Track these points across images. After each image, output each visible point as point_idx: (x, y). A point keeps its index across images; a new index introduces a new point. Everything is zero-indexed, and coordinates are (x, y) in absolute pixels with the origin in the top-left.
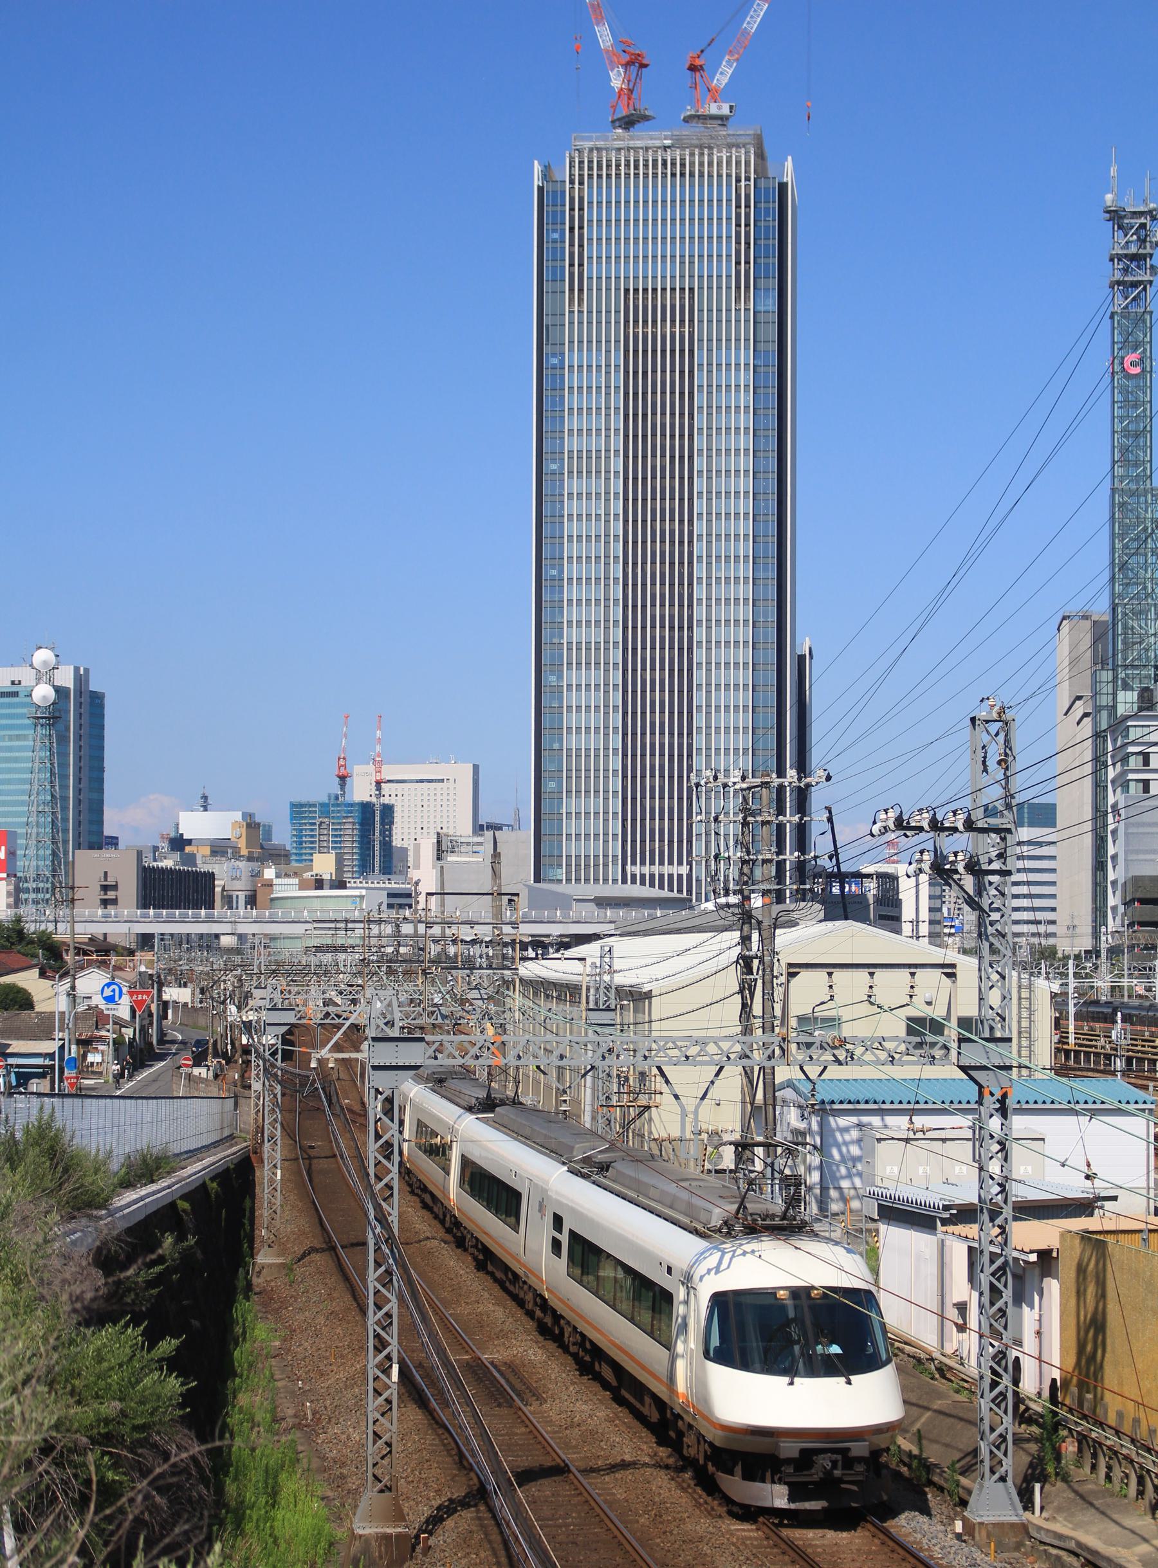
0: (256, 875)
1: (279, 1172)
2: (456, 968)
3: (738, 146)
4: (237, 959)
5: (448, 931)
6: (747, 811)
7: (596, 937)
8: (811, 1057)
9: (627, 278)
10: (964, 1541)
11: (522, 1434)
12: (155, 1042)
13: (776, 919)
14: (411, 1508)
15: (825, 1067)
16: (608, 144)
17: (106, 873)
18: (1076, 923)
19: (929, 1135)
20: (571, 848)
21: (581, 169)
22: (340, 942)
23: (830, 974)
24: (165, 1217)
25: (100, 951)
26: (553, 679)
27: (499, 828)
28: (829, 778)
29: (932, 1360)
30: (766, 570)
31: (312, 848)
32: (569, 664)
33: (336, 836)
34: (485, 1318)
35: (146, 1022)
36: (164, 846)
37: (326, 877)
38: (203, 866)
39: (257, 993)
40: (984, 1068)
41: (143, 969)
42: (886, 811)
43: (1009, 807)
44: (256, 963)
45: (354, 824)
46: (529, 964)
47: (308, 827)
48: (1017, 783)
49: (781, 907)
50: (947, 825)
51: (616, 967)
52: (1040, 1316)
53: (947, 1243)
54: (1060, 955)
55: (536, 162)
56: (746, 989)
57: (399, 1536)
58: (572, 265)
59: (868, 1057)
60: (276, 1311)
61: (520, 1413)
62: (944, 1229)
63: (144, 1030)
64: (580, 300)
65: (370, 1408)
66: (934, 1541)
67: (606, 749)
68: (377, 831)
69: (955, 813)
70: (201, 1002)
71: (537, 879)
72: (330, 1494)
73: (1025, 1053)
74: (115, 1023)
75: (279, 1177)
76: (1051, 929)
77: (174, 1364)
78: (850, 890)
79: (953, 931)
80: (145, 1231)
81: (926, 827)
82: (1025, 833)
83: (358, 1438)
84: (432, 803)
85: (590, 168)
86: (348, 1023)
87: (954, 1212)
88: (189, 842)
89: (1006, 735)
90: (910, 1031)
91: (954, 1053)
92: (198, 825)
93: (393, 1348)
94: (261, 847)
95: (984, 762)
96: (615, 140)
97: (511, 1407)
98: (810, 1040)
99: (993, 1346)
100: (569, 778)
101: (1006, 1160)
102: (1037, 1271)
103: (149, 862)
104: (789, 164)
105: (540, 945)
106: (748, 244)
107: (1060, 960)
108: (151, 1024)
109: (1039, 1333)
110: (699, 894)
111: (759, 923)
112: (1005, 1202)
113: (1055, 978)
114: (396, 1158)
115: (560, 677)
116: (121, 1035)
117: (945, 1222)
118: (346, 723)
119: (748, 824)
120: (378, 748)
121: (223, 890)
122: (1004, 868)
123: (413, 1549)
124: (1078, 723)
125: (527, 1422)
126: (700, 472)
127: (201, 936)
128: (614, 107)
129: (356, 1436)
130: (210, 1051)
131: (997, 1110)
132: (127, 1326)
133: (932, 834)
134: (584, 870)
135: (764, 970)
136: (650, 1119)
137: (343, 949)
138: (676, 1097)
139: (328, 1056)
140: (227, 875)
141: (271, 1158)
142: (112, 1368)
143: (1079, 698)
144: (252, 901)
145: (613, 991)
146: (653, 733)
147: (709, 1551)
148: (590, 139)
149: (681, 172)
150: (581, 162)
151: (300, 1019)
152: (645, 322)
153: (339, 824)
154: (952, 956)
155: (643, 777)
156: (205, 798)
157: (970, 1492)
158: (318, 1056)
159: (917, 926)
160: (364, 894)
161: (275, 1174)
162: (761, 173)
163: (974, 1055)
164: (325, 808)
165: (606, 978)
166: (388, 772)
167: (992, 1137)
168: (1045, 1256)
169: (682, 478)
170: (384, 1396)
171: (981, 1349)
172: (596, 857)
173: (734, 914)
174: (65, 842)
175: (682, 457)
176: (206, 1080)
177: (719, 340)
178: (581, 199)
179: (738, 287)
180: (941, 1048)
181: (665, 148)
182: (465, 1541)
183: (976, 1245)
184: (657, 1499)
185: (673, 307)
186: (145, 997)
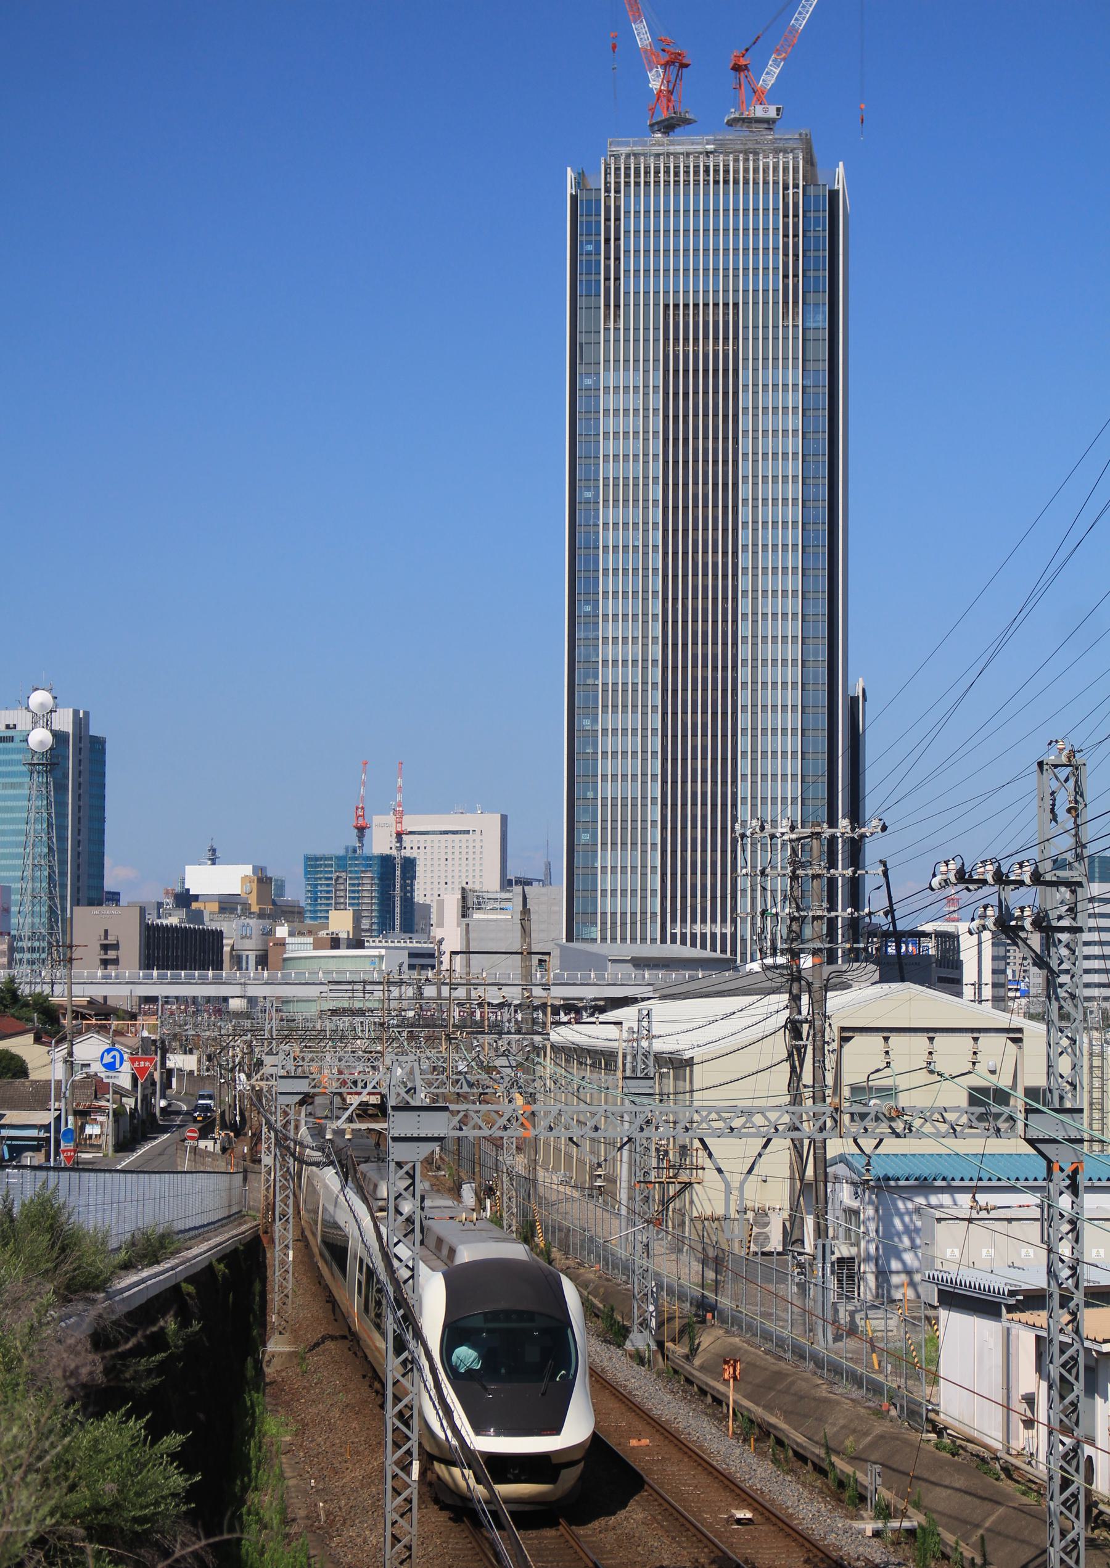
0: (269, 933)
1: (291, 1253)
3: (785, 151)
4: (247, 1024)
5: (474, 994)
6: (796, 864)
8: (866, 1130)
9: (666, 292)
13: (828, 980)
15: (881, 1140)
16: (647, 149)
17: (106, 931)
19: (994, 1214)
20: (605, 905)
21: (617, 176)
22: (358, 1005)
24: (169, 1298)
25: (100, 1014)
26: (587, 723)
27: (528, 883)
28: (884, 828)
29: (997, 1459)
30: (815, 606)
31: (328, 905)
32: (605, 706)
33: (353, 891)
38: (210, 925)
39: (268, 1060)
40: (1054, 1141)
41: (145, 1034)
42: (947, 863)
43: (1079, 857)
44: (267, 1027)
45: (372, 878)
46: (562, 1029)
48: (1088, 832)
49: (832, 968)
50: (1012, 878)
51: (655, 1032)
53: (1013, 1332)
55: (569, 169)
56: (795, 1055)
58: (607, 279)
59: (928, 1128)
60: (288, 1404)
62: (1010, 1316)
63: (146, 1100)
65: (388, 1509)
67: (644, 798)
68: (398, 886)
70: (208, 1070)
71: (570, 938)
74: (115, 1092)
75: (291, 1259)
77: (183, 1459)
81: (990, 880)
83: (374, 1542)
85: (627, 175)
87: (1021, 1298)
88: (196, 898)
89: (1076, 782)
91: (1020, 1125)
92: (212, 880)
94: (270, 901)
96: (654, 145)
98: (864, 1110)
99: (1063, 1444)
100: (604, 829)
101: (1077, 1241)
103: (152, 919)
104: (840, 170)
105: (574, 1009)
106: (796, 255)
110: (744, 954)
112: (1077, 1287)
116: (122, 1105)
117: (1010, 1309)
121: (232, 949)
127: (208, 999)
128: (653, 110)
131: (1067, 1187)
133: (996, 888)
134: (622, 927)
135: (814, 1036)
137: (361, 1012)
138: (720, 1171)
139: (345, 1126)
140: (234, 933)
141: (283, 1238)
142: (110, 1459)
144: (263, 961)
145: (652, 1058)
148: (627, 144)
149: (724, 179)
150: (617, 169)
151: (314, 1087)
153: (358, 878)
154: (1018, 1021)
155: (684, 782)
158: (334, 1127)
159: (980, 989)
160: (383, 954)
161: (287, 1255)
163: (1045, 1126)
164: (342, 862)
165: (644, 1044)
166: (410, 823)
167: (1062, 1216)
171: (1051, 1447)
174: (63, 898)
176: (213, 1153)
177: (765, 359)
180: (1006, 1120)
181: (708, 154)
183: (1044, 1334)
185: (716, 323)
186: (147, 1064)
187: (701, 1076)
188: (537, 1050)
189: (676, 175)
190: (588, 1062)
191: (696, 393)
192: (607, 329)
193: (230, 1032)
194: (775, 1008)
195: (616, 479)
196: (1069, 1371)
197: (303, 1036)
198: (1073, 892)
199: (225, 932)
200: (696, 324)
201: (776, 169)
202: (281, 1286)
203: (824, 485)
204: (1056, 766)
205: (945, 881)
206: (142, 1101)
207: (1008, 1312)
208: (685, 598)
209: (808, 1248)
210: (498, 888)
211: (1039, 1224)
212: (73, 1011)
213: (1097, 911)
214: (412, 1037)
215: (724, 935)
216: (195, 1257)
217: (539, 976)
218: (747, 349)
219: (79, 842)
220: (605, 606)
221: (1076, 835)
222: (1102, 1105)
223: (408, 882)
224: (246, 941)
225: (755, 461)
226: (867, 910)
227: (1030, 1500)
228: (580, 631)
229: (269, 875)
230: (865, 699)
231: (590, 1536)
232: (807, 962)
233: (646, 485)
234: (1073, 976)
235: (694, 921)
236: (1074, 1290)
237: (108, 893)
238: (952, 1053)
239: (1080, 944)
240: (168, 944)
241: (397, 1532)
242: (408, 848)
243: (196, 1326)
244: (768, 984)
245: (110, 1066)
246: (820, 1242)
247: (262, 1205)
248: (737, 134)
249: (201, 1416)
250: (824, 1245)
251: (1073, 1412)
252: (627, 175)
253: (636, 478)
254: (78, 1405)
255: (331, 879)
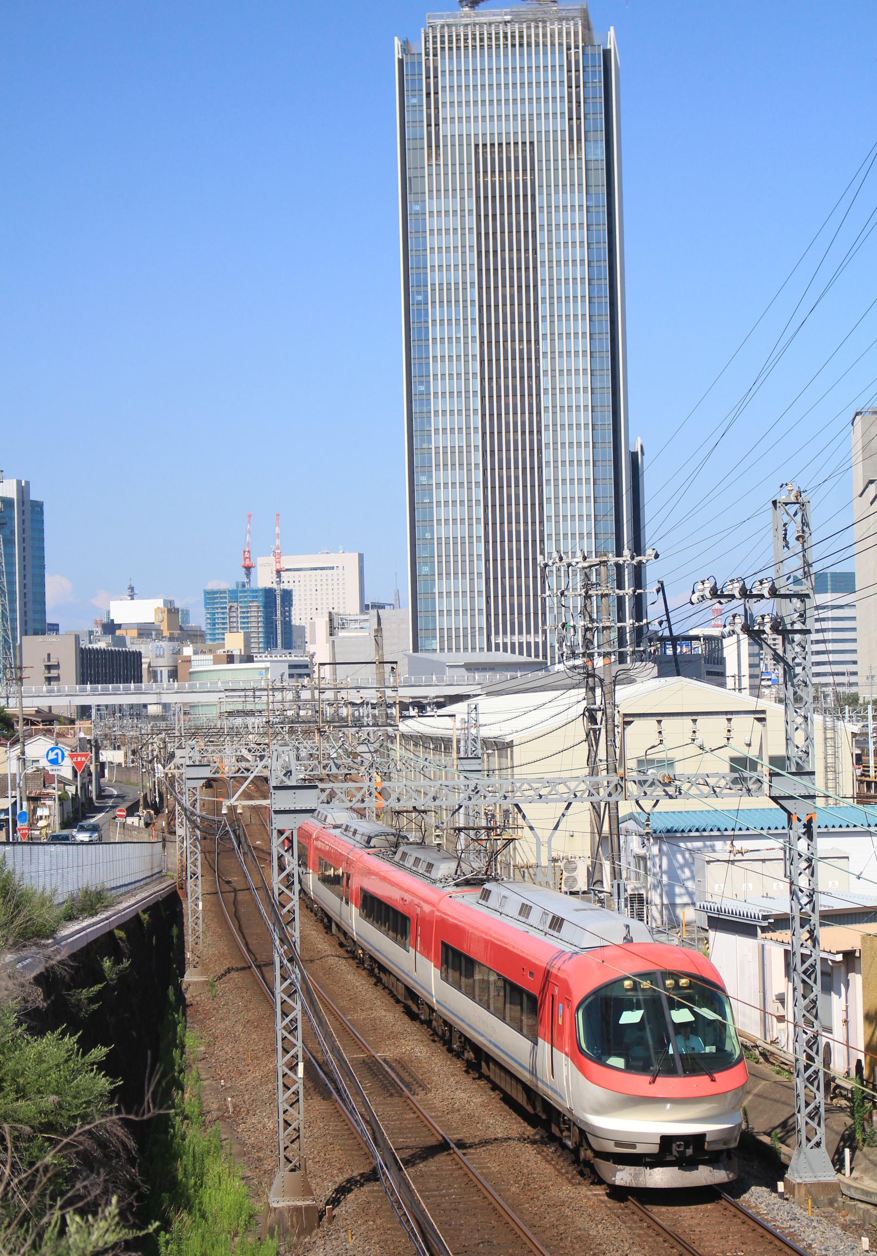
0: (179, 652)
1: (200, 904)
2: (347, 726)
3: (567, 19)
4: (162, 725)
6: (587, 586)
7: (468, 697)
8: (645, 793)
10: (787, 1199)
11: (412, 1119)
12: (94, 798)
13: (616, 677)
14: (318, 1184)
15: (657, 801)
16: (457, 21)
17: (49, 655)
18: (874, 673)
19: (747, 856)
20: (443, 622)
21: (435, 43)
22: (249, 707)
23: (659, 722)
24: (105, 943)
25: (46, 720)
27: (382, 607)
28: (657, 556)
29: (757, 1046)
31: (223, 629)
32: (437, 465)
33: (244, 618)
34: (378, 1022)
35: (86, 780)
36: (99, 630)
37: (236, 653)
38: (132, 648)
39: (178, 753)
40: (791, 798)
41: (82, 735)
42: (703, 582)
43: (806, 575)
45: (258, 607)
46: (409, 722)
47: (219, 611)
48: (812, 555)
49: (623, 666)
50: (755, 592)
51: (481, 722)
52: (847, 1007)
53: (767, 947)
54: (861, 701)
55: (396, 38)
56: (592, 737)
57: (308, 1208)
58: (428, 77)
59: (694, 791)
60: (202, 1022)
61: (409, 1101)
62: (764, 935)
63: (85, 788)
64: (438, 155)
65: (280, 1100)
66: (760, 1200)
67: (471, 537)
68: (279, 612)
69: (761, 583)
71: (416, 649)
72: (249, 1174)
73: (831, 784)
74: (59, 782)
75: (200, 908)
76: (853, 679)
77: (107, 1067)
78: (681, 651)
79: (769, 683)
80: (87, 957)
81: (737, 595)
82: (820, 599)
83: (272, 1127)
84: (324, 587)
85: (443, 42)
86: (252, 776)
87: (772, 921)
88: (119, 626)
89: (803, 515)
90: (733, 770)
91: (766, 786)
92: (131, 612)
93: (299, 1049)
94: (178, 628)
95: (785, 538)
96: (462, 17)
97: (401, 1096)
98: (645, 778)
99: (806, 1033)
100: (440, 562)
101: (812, 875)
102: (843, 969)
103: (85, 644)
104: (612, 33)
106: (578, 102)
107: (861, 705)
108: (90, 782)
109: (846, 1022)
110: (553, 658)
111: (601, 681)
112: (813, 911)
113: (858, 721)
114: (297, 887)
115: (430, 477)
117: (764, 930)
118: (249, 522)
119: (590, 597)
120: (278, 542)
121: (149, 666)
122: (804, 628)
123: (320, 1218)
124: (871, 503)
125: (415, 1109)
126: (549, 499)
127: (132, 706)
129: (270, 1125)
130: (141, 803)
131: (804, 834)
132: (63, 1033)
133: (742, 601)
134: (456, 640)
135: (606, 720)
136: (515, 848)
137: (251, 713)
138: (531, 828)
139: (236, 803)
140: (153, 654)
142: (51, 1068)
143: (871, 482)
144: (174, 674)
145: (479, 742)
146: (510, 522)
147: (570, 1213)
148: (441, 17)
149: (519, 43)
150: (435, 37)
151: (214, 773)
152: (493, 172)
153: (247, 607)
154: (762, 704)
155: (502, 541)
156: (132, 589)
157: (790, 1158)
159: (740, 680)
160: (269, 666)
162: (588, 41)
163: (786, 785)
164: (234, 595)
165: (473, 731)
166: (287, 562)
168: (850, 957)
169: (528, 305)
170: (293, 1089)
172: (465, 629)
173: (579, 674)
174: (14, 629)
175: (528, 287)
176: (138, 828)
177: (556, 186)
178: (436, 69)
179: (571, 140)
180: (755, 783)
181: (506, 23)
182: (364, 1210)
183: (789, 948)
184: (525, 1171)
185: (516, 158)
186: (83, 759)
187: (519, 755)
188: (392, 739)
189: (480, 42)
190: (431, 747)
191: (502, 214)
192: (430, 165)
193: (149, 731)
194: (575, 699)
195: (441, 284)
196: (809, 977)
197: (210, 734)
198: (803, 601)
199: (143, 652)
200: (501, 159)
201: (560, 34)
202: (194, 929)
203: (605, 284)
204: (786, 504)
205: (702, 596)
206: (81, 788)
207: (763, 932)
208: (498, 378)
209: (607, 887)
210: (358, 612)
211: (783, 862)
212: (24, 719)
213: (821, 616)
214: (292, 731)
215: (536, 644)
216: (124, 909)
217: (392, 680)
218: (542, 178)
219: (25, 585)
220: (435, 386)
221: (804, 556)
222: (835, 768)
223: (287, 609)
224: (160, 659)
225: (551, 267)
226: (645, 621)
227: (783, 1078)
228: (416, 406)
229: (177, 605)
230: (643, 454)
231: (441, 1117)
232: (599, 662)
233: (464, 289)
234: (804, 669)
235: (512, 633)
236: (811, 914)
237: (49, 624)
238: (711, 730)
239: (809, 642)
240: (98, 663)
241: (288, 1119)
242: (286, 582)
243: (126, 963)
244: (569, 681)
245: (54, 762)
246: (616, 882)
247: (178, 867)
248: (529, 6)
249: (134, 1034)
250: (619, 885)
251: (813, 1008)
252: (443, 42)
253: (456, 284)
254: (25, 1026)
255: (225, 608)
